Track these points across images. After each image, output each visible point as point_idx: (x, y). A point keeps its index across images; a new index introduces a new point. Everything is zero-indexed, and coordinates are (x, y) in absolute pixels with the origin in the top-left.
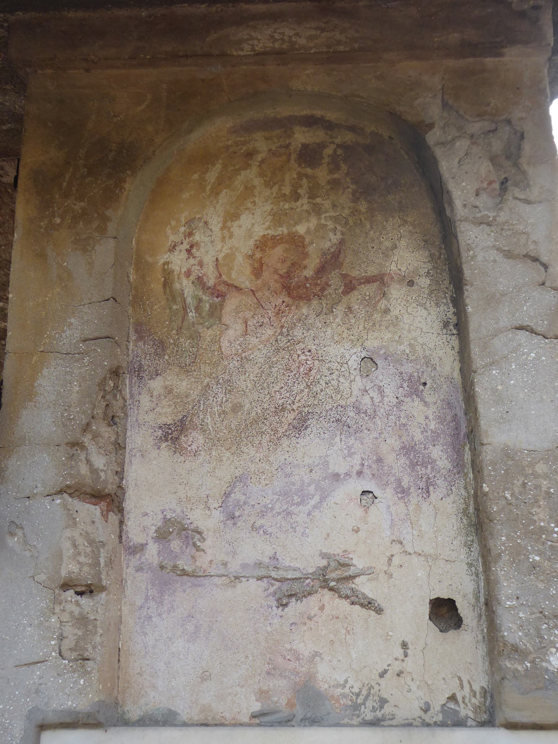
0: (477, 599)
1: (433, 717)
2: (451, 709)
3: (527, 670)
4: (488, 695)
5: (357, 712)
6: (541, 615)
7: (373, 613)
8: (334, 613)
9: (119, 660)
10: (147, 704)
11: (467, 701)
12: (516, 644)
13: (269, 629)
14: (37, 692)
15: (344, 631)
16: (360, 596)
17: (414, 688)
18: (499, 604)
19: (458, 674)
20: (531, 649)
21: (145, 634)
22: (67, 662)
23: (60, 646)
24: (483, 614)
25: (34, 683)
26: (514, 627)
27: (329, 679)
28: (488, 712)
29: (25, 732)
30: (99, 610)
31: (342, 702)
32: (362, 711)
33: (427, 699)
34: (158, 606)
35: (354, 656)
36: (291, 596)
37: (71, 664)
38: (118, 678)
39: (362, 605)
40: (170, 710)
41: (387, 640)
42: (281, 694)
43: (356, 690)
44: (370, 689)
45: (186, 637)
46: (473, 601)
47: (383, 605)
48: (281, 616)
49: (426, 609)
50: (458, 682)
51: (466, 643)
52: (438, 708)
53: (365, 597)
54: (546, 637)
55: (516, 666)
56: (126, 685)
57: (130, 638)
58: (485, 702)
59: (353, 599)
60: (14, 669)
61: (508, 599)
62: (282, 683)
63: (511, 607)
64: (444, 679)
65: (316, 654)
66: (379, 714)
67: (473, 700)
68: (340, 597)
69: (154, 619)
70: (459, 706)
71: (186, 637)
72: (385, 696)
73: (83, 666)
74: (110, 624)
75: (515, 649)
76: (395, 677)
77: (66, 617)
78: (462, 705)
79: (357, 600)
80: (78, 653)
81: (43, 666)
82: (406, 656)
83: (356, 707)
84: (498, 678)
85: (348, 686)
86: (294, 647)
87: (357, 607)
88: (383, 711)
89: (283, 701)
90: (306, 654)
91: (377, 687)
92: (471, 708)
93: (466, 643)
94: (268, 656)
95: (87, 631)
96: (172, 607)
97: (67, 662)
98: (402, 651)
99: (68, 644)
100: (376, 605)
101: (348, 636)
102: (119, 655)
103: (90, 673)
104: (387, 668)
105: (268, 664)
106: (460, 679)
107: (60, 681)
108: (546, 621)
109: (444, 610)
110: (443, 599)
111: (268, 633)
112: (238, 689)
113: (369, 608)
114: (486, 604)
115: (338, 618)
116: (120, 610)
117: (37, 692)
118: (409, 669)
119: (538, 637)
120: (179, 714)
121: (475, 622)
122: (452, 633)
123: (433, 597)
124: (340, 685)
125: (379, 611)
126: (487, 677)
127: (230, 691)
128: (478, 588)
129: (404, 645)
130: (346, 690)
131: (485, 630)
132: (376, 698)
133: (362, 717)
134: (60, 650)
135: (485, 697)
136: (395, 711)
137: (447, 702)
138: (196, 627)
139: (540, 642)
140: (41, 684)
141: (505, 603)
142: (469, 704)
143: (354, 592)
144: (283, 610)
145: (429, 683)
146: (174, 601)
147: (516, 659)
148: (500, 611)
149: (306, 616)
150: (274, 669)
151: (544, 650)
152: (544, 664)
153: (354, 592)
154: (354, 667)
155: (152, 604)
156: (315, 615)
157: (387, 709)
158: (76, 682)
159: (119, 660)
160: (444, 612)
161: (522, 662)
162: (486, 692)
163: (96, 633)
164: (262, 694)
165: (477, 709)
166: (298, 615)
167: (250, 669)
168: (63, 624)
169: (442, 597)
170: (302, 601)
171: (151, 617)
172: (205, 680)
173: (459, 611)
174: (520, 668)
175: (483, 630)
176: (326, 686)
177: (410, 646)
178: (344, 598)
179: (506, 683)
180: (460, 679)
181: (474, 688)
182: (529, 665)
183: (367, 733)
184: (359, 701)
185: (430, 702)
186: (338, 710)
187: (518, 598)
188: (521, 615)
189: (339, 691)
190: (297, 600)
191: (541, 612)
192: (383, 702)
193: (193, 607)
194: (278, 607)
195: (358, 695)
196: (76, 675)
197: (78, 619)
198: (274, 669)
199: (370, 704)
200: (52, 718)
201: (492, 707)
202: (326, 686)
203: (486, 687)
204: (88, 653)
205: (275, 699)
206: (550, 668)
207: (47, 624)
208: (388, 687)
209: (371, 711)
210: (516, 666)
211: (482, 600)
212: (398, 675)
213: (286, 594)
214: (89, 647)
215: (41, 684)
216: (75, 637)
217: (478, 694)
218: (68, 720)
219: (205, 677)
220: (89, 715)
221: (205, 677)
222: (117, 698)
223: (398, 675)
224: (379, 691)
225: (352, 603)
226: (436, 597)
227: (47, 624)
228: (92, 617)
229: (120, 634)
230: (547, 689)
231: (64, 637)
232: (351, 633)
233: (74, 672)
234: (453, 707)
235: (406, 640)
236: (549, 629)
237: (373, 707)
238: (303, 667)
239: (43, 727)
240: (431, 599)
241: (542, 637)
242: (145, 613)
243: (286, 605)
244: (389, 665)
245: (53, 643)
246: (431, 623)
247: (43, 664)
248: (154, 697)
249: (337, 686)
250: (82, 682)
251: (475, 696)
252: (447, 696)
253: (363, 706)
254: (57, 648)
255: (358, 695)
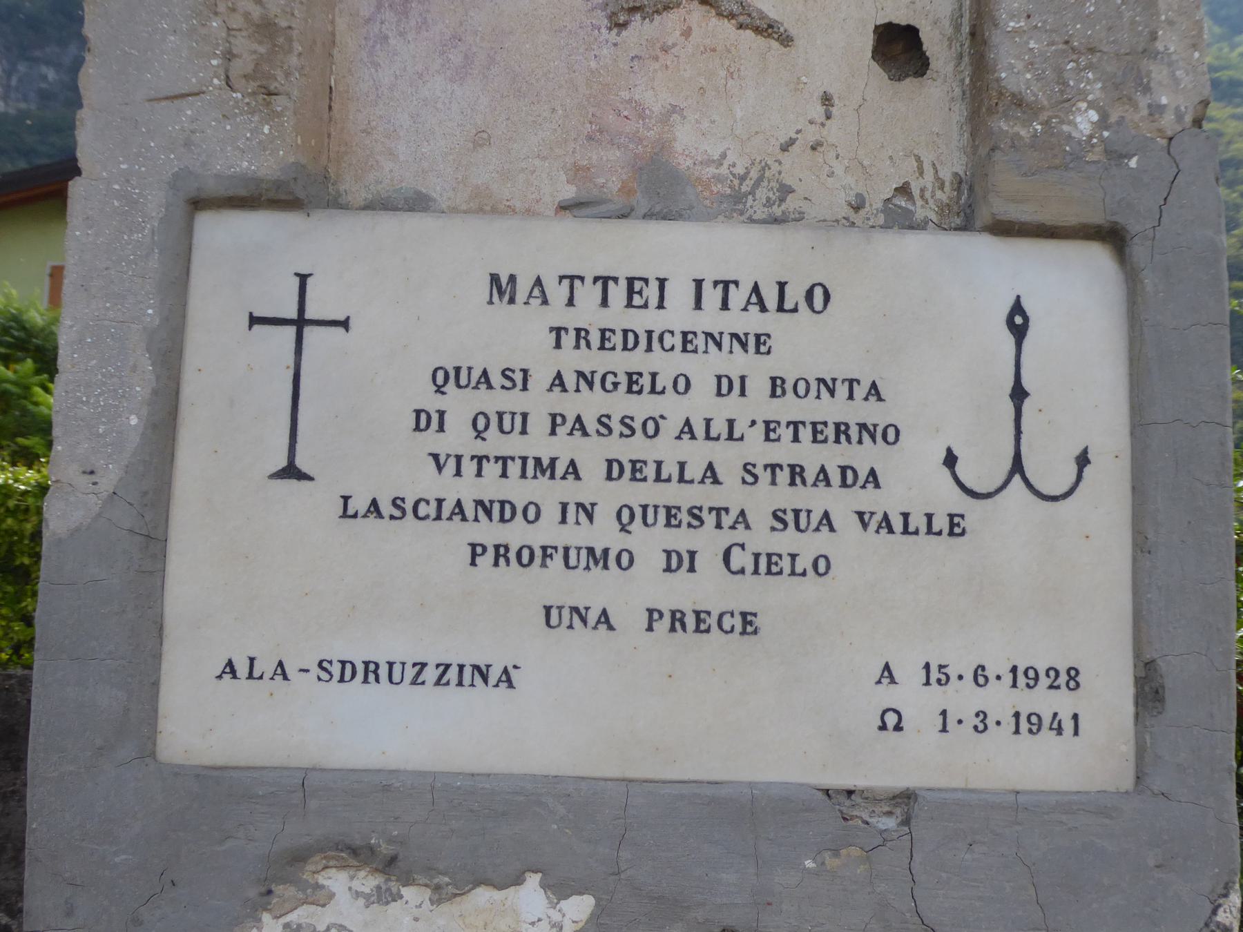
0: (957, 27)
1: (868, 219)
2: (900, 207)
3: (1035, 136)
4: (965, 187)
5: (741, 206)
6: (1064, 47)
7: (775, 44)
8: (707, 41)
9: (330, 108)
10: (379, 182)
11: (928, 195)
12: (1020, 93)
13: (593, 64)
14: (187, 144)
15: (723, 73)
16: (754, 14)
17: (839, 169)
18: (996, 25)
19: (916, 152)
20: (1046, 103)
21: (376, 65)
22: (239, 95)
23: (227, 71)
24: (966, 54)
25: (183, 129)
26: (1019, 65)
27: (694, 151)
28: (962, 214)
29: (167, 210)
30: (296, 12)
31: (715, 189)
32: (748, 205)
33: (860, 189)
34: (399, 21)
35: (739, 114)
36: (633, 10)
37: (247, 100)
38: (329, 136)
39: (757, 30)
40: (418, 193)
41: (796, 90)
42: (611, 169)
43: (740, 170)
44: (763, 169)
45: (448, 73)
46: (949, 31)
47: (793, 32)
48: (615, 45)
49: (868, 41)
50: (915, 164)
51: (934, 102)
52: (880, 205)
53: (763, 16)
54: (1071, 83)
55: (1016, 129)
56: (343, 149)
57: (350, 71)
58: (959, 198)
59: (741, 19)
60: (147, 104)
61: (1012, 17)
62: (614, 155)
63: (1015, 31)
64: (891, 158)
65: (674, 109)
66: (777, 211)
67: (939, 194)
68: (720, 15)
69: (392, 41)
70: (914, 204)
71: (448, 73)
72: (788, 181)
73: (268, 104)
74: (315, 42)
75: (1018, 102)
76: (809, 151)
77: (237, 21)
78: (919, 203)
79: (749, 20)
80: (259, 83)
81: (197, 102)
82: (828, 118)
83: (738, 198)
84: (983, 151)
85: (726, 163)
86: (637, 97)
87: (749, 33)
88: (783, 207)
89: (614, 185)
90: (657, 109)
91: (775, 167)
92: (934, 207)
93: (934, 102)
94: (591, 110)
95: (275, 45)
96: (425, 22)
97: (239, 95)
98: (821, 110)
99: (240, 67)
100: (782, 30)
101: (731, 82)
102: (331, 99)
103: (279, 115)
104: (794, 136)
105: (591, 123)
106: (918, 159)
107: (228, 127)
108: (1075, 57)
109: (898, 47)
110: (898, 25)
111: (592, 72)
112: (537, 162)
113: (769, 36)
114: (973, 34)
115: (714, 50)
116: (333, 22)
117: (187, 144)
118: (832, 140)
119: (1058, 83)
120: (435, 200)
121: (950, 68)
122: (909, 83)
123: (880, 22)
124: (713, 161)
125: (786, 40)
126: (965, 159)
127: (523, 165)
128: (960, 9)
129: (827, 100)
130: (724, 170)
131: (967, 81)
132: (774, 184)
133: (747, 215)
134: (228, 77)
135: (959, 189)
136: (805, 207)
137: (893, 196)
138: (466, 57)
139: (1062, 92)
140: (193, 132)
141: (1006, 25)
142: (931, 201)
143: (743, 8)
144: (618, 34)
145: (866, 163)
146: (428, 11)
147: (1018, 118)
148: (996, 38)
149: (658, 45)
150: (601, 131)
151: (1066, 105)
152: (1065, 128)
153: (743, 8)
154: (737, 132)
155: (388, 15)
156: (674, 45)
157: (792, 203)
158: (256, 131)
159: (330, 108)
160: (898, 47)
161: (1027, 123)
162: (960, 182)
163: (290, 51)
164: (579, 172)
165: (943, 209)
166: (644, 43)
167: (559, 131)
168: (233, 33)
169: (896, 21)
170: (652, 21)
171: (386, 38)
172: (481, 146)
173: (925, 48)
174: (1023, 133)
175: (962, 81)
176: (689, 162)
177: (836, 101)
178: (727, 17)
179: (998, 155)
180: (918, 159)
181: (941, 175)
182: (1039, 127)
183: (757, 232)
184: (744, 188)
185: (865, 194)
186: (707, 202)
187: (1029, 17)
188: (1032, 45)
189: (712, 170)
190: (644, 19)
191: (1067, 42)
192: (786, 191)
193: (461, 24)
194: (610, 29)
195: (743, 178)
196: (256, 118)
197: (258, 26)
198: (601, 131)
199: (762, 194)
200: (213, 188)
201: (970, 206)
202: (689, 162)
203: (961, 173)
204: (276, 84)
205: (601, 180)
206: (1074, 134)
207: (203, 31)
208: (794, 169)
209: (764, 206)
210: (1016, 129)
211: (966, 29)
212: (813, 148)
213: (626, 6)
214: (279, 74)
215: (193, 132)
216: (254, 57)
217: (947, 184)
218: (243, 192)
219: (480, 140)
220: (279, 185)
221: (480, 140)
222: (326, 168)
223: (813, 148)
224: (780, 173)
225: (741, 27)
226: (886, 21)
227: (203, 31)
228: (284, 24)
229: (333, 63)
230: (1067, 168)
231: (235, 56)
232: (735, 76)
233: (253, 113)
234: (903, 204)
235: (831, 91)
236: (1079, 70)
237: (768, 199)
238: (650, 129)
239: (198, 204)
240: (878, 23)
241: (1065, 84)
242: (376, 30)
243: (624, 25)
244: (798, 132)
245: (214, 62)
246: (874, 65)
247: (197, 98)
248: (391, 171)
249: (709, 162)
250: (266, 129)
251: (942, 187)
252: (895, 186)
253: (750, 197)
254: (221, 72)
255: (743, 178)
